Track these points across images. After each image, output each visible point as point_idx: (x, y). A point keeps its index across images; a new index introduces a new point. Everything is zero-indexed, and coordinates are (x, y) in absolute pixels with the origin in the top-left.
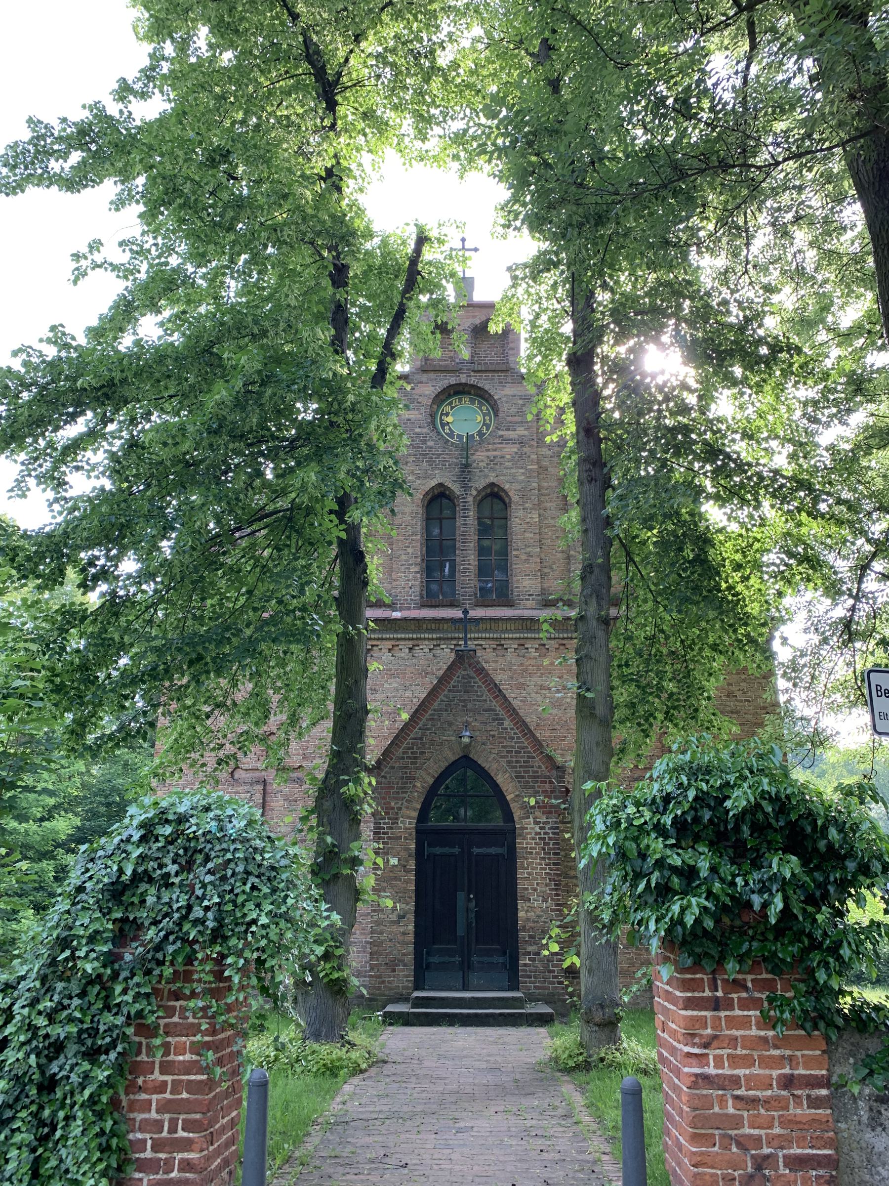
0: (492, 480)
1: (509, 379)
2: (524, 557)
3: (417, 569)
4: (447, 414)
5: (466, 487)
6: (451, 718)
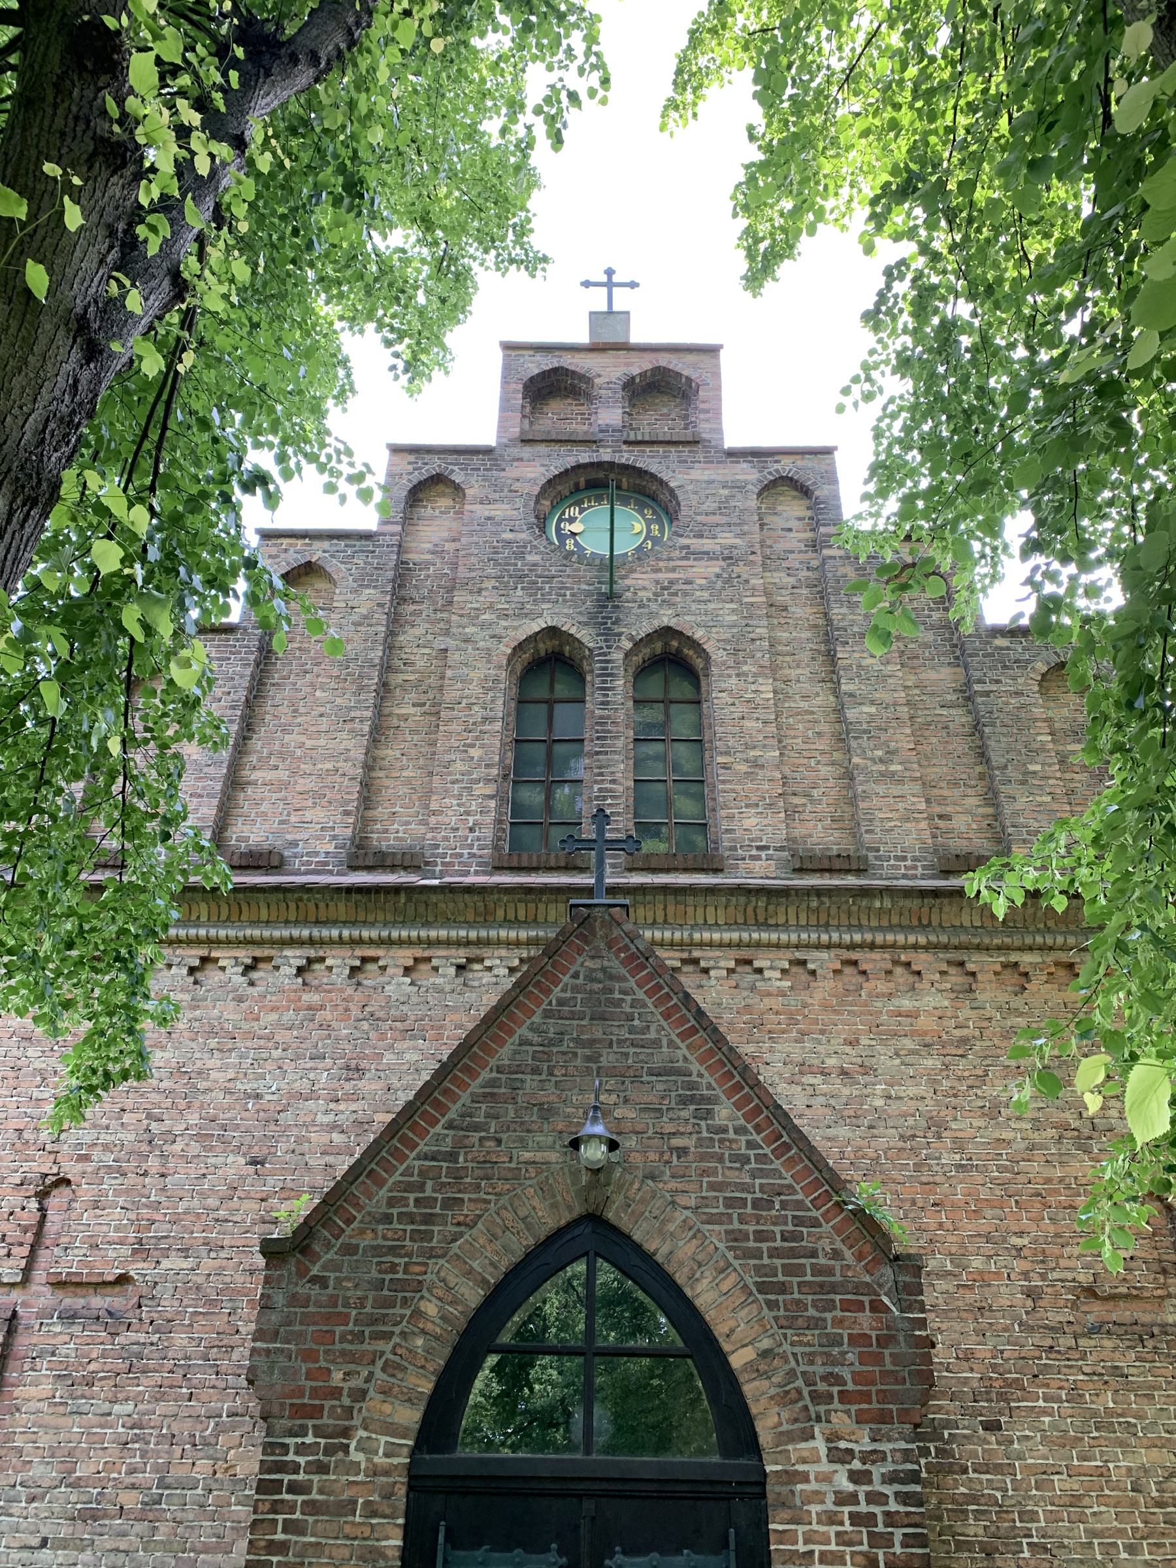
0: (665, 621)
1: (700, 457)
2: (743, 768)
3: (490, 789)
4: (572, 520)
5: (609, 635)
6: (549, 1095)
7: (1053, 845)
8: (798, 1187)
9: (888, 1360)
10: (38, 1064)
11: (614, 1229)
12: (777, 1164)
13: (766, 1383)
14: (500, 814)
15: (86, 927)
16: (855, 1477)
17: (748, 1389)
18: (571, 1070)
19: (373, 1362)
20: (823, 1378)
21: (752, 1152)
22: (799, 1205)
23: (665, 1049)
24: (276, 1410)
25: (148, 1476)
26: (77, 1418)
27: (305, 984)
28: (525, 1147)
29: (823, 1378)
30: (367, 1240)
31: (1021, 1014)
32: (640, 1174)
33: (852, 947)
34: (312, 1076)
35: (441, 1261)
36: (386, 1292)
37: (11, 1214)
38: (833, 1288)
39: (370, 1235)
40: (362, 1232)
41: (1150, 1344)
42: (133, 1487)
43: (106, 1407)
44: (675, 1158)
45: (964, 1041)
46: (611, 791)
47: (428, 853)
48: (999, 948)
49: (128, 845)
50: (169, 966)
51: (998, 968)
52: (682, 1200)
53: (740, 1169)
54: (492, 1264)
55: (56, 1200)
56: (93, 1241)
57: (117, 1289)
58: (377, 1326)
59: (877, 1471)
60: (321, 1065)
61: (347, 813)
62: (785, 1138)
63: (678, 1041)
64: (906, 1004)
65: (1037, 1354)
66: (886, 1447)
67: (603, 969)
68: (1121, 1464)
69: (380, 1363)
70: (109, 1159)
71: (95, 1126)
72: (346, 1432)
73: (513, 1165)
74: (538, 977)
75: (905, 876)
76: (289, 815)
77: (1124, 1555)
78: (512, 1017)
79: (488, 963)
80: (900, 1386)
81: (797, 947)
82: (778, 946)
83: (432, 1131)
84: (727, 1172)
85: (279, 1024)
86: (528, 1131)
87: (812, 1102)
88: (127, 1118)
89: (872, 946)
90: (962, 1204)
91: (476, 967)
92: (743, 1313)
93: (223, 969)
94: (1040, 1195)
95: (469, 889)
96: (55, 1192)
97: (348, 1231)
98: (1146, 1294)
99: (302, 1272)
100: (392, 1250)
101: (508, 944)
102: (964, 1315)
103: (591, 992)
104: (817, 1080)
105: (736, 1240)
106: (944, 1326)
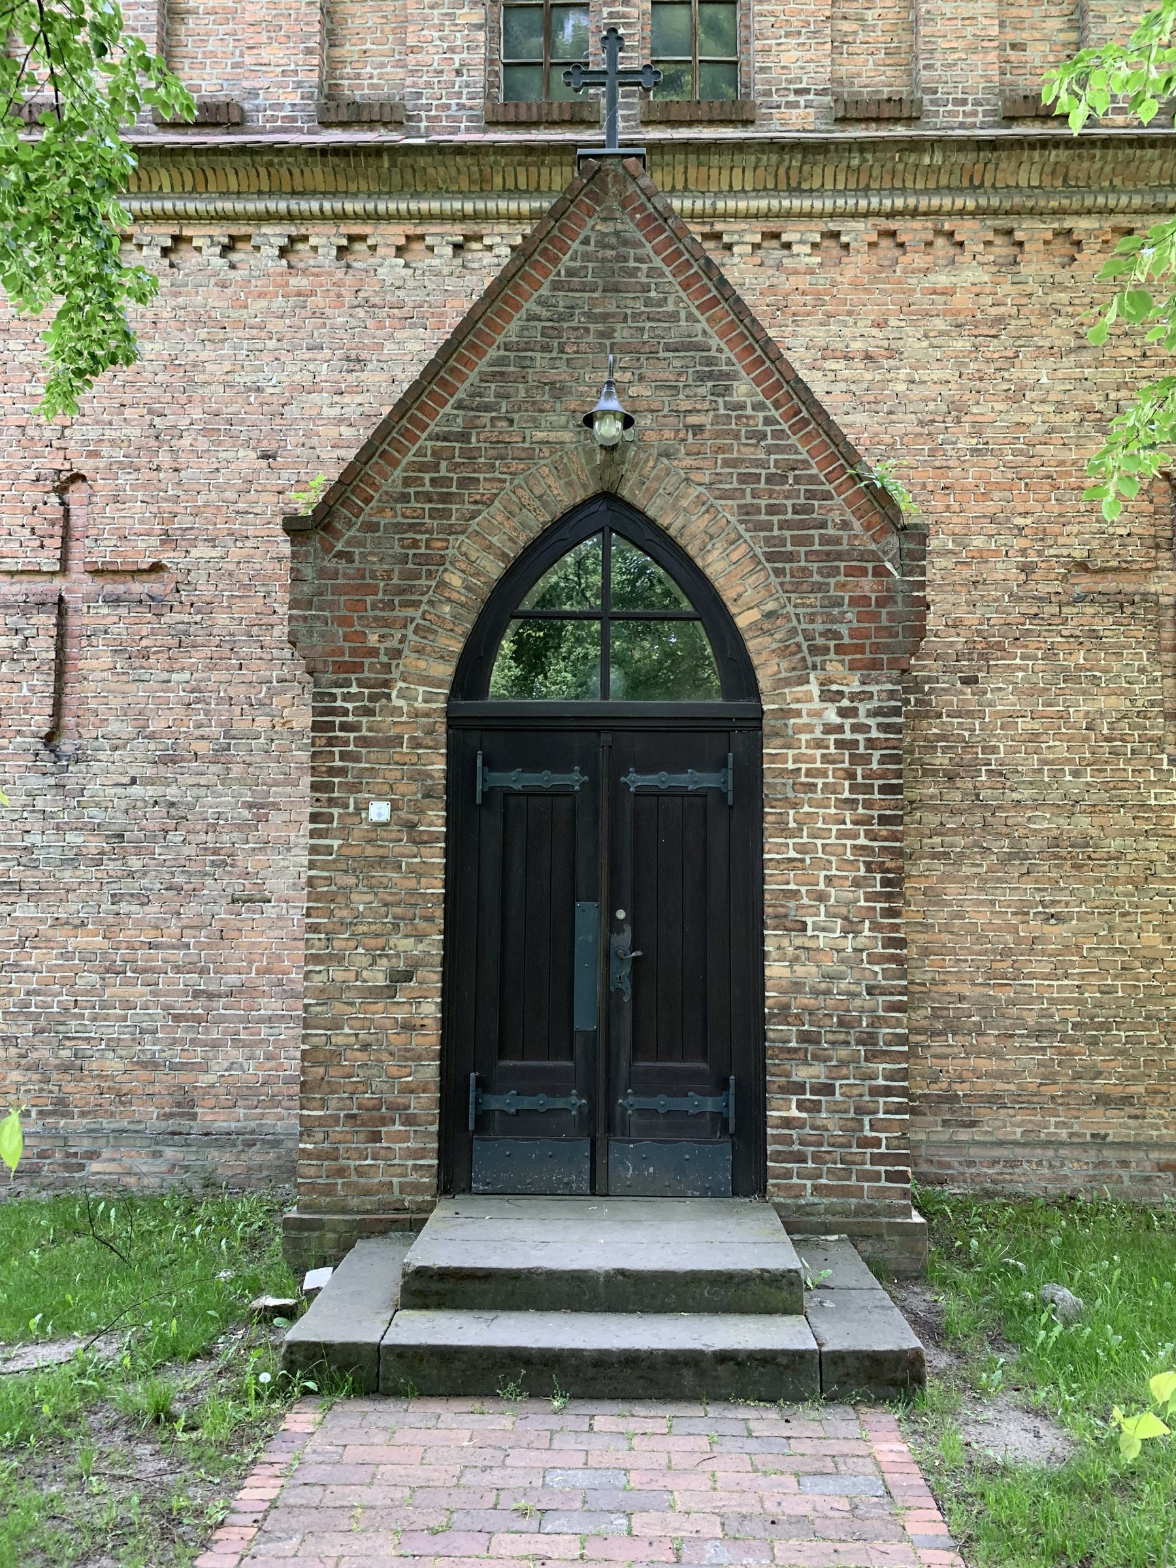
6: (561, 373)
7: (1157, 29)
8: (812, 462)
9: (884, 617)
10: (22, 358)
11: (629, 506)
12: (793, 440)
13: (769, 639)
14: (491, 51)
15: (33, 176)
16: (842, 713)
17: (751, 645)
18: (583, 347)
19: (405, 626)
20: (821, 634)
21: (769, 429)
22: (813, 479)
23: (683, 323)
24: (320, 666)
25: (215, 730)
26: (141, 685)
27: (290, 266)
28: (537, 427)
29: (821, 634)
30: (386, 518)
31: (1065, 289)
32: (655, 452)
33: (892, 214)
34: (311, 367)
35: (461, 537)
36: (410, 566)
37: (35, 508)
38: (839, 556)
39: (389, 513)
40: (381, 510)
41: (1129, 610)
42: (202, 738)
43: (165, 676)
44: (690, 436)
45: (999, 320)
46: (624, 16)
47: (409, 104)
48: (1054, 212)
49: (58, 70)
50: (140, 247)
51: (1049, 235)
52: (696, 477)
53: (756, 446)
54: (511, 539)
55: (76, 494)
56: (120, 532)
57: (153, 576)
58: (405, 595)
59: (863, 708)
60: (319, 357)
61: (309, 52)
62: (805, 414)
63: (697, 313)
64: (942, 279)
65: (1022, 620)
66: (874, 688)
67: (617, 234)
68: (1080, 709)
69: (411, 627)
70: (119, 455)
71: (97, 423)
72: (387, 684)
73: (527, 445)
74: (545, 244)
75: (962, 126)
76: (242, 55)
77: (1069, 778)
78: (517, 289)
79: (487, 241)
80: (892, 636)
81: (831, 216)
82: (810, 215)
83: (442, 411)
84: (743, 449)
85: (268, 312)
86: (541, 411)
87: (832, 388)
88: (128, 413)
89: (914, 213)
90: (972, 487)
91: (475, 246)
92: (751, 580)
93: (198, 249)
94: (1051, 477)
95: (460, 150)
96: (72, 488)
97: (367, 509)
98: (1135, 567)
99: (328, 548)
100: (412, 527)
101: (509, 218)
102: (958, 588)
103: (604, 260)
104: (841, 364)
105: (748, 514)
106: (937, 599)
